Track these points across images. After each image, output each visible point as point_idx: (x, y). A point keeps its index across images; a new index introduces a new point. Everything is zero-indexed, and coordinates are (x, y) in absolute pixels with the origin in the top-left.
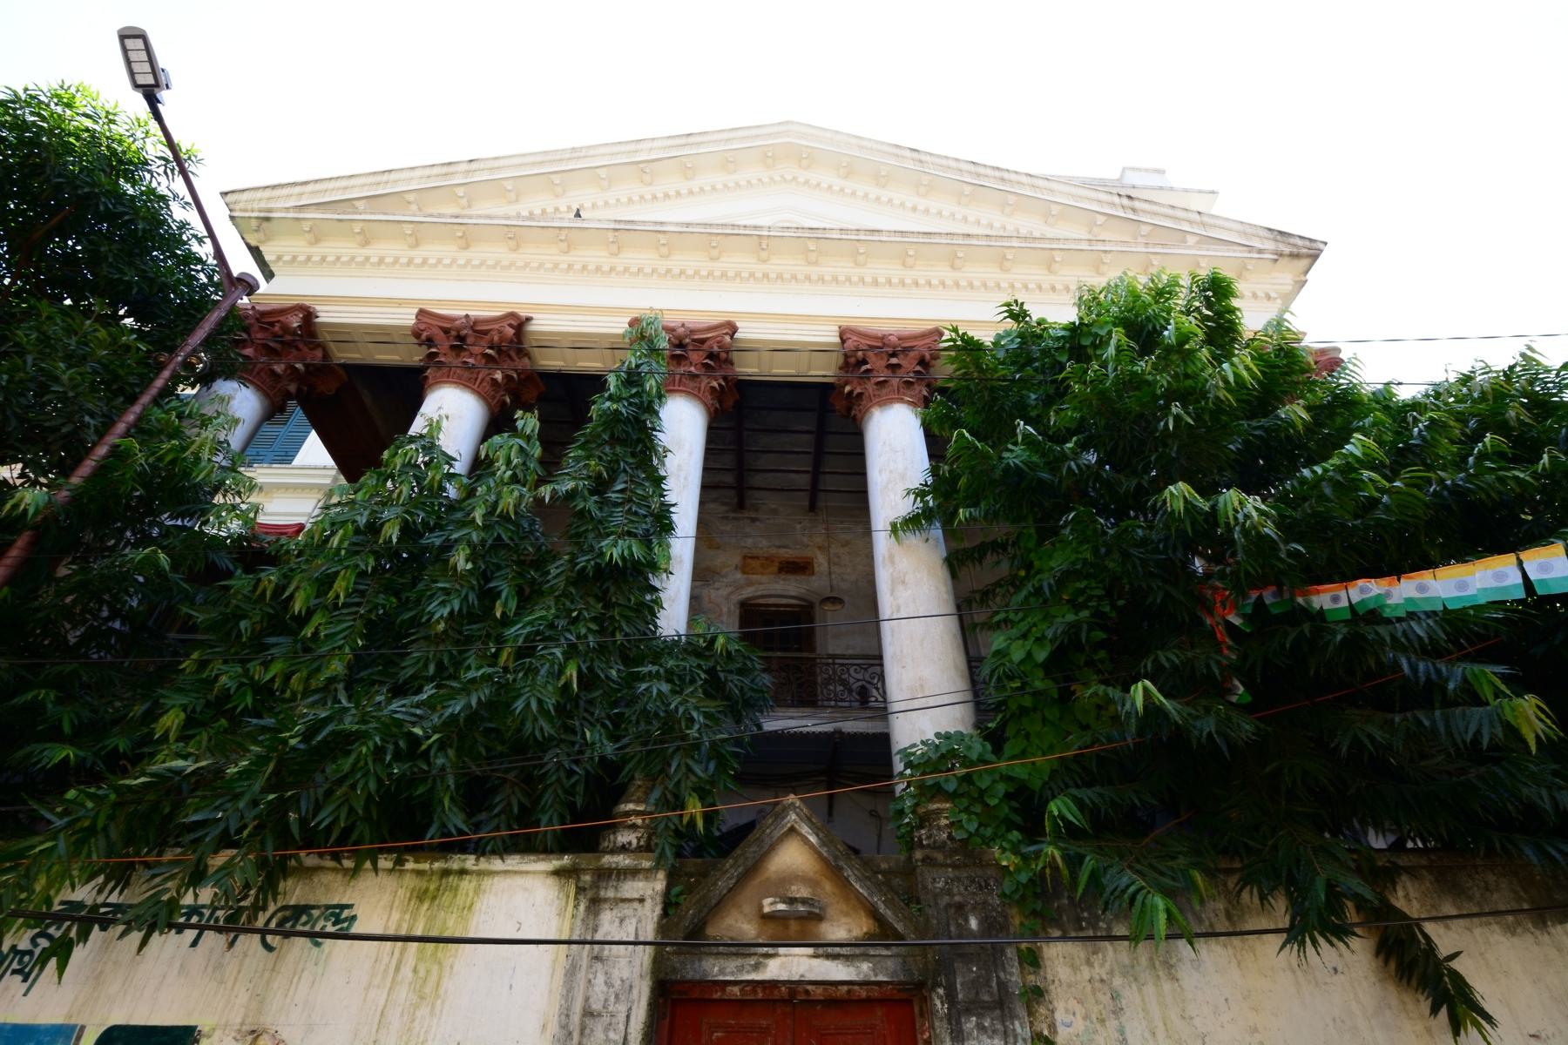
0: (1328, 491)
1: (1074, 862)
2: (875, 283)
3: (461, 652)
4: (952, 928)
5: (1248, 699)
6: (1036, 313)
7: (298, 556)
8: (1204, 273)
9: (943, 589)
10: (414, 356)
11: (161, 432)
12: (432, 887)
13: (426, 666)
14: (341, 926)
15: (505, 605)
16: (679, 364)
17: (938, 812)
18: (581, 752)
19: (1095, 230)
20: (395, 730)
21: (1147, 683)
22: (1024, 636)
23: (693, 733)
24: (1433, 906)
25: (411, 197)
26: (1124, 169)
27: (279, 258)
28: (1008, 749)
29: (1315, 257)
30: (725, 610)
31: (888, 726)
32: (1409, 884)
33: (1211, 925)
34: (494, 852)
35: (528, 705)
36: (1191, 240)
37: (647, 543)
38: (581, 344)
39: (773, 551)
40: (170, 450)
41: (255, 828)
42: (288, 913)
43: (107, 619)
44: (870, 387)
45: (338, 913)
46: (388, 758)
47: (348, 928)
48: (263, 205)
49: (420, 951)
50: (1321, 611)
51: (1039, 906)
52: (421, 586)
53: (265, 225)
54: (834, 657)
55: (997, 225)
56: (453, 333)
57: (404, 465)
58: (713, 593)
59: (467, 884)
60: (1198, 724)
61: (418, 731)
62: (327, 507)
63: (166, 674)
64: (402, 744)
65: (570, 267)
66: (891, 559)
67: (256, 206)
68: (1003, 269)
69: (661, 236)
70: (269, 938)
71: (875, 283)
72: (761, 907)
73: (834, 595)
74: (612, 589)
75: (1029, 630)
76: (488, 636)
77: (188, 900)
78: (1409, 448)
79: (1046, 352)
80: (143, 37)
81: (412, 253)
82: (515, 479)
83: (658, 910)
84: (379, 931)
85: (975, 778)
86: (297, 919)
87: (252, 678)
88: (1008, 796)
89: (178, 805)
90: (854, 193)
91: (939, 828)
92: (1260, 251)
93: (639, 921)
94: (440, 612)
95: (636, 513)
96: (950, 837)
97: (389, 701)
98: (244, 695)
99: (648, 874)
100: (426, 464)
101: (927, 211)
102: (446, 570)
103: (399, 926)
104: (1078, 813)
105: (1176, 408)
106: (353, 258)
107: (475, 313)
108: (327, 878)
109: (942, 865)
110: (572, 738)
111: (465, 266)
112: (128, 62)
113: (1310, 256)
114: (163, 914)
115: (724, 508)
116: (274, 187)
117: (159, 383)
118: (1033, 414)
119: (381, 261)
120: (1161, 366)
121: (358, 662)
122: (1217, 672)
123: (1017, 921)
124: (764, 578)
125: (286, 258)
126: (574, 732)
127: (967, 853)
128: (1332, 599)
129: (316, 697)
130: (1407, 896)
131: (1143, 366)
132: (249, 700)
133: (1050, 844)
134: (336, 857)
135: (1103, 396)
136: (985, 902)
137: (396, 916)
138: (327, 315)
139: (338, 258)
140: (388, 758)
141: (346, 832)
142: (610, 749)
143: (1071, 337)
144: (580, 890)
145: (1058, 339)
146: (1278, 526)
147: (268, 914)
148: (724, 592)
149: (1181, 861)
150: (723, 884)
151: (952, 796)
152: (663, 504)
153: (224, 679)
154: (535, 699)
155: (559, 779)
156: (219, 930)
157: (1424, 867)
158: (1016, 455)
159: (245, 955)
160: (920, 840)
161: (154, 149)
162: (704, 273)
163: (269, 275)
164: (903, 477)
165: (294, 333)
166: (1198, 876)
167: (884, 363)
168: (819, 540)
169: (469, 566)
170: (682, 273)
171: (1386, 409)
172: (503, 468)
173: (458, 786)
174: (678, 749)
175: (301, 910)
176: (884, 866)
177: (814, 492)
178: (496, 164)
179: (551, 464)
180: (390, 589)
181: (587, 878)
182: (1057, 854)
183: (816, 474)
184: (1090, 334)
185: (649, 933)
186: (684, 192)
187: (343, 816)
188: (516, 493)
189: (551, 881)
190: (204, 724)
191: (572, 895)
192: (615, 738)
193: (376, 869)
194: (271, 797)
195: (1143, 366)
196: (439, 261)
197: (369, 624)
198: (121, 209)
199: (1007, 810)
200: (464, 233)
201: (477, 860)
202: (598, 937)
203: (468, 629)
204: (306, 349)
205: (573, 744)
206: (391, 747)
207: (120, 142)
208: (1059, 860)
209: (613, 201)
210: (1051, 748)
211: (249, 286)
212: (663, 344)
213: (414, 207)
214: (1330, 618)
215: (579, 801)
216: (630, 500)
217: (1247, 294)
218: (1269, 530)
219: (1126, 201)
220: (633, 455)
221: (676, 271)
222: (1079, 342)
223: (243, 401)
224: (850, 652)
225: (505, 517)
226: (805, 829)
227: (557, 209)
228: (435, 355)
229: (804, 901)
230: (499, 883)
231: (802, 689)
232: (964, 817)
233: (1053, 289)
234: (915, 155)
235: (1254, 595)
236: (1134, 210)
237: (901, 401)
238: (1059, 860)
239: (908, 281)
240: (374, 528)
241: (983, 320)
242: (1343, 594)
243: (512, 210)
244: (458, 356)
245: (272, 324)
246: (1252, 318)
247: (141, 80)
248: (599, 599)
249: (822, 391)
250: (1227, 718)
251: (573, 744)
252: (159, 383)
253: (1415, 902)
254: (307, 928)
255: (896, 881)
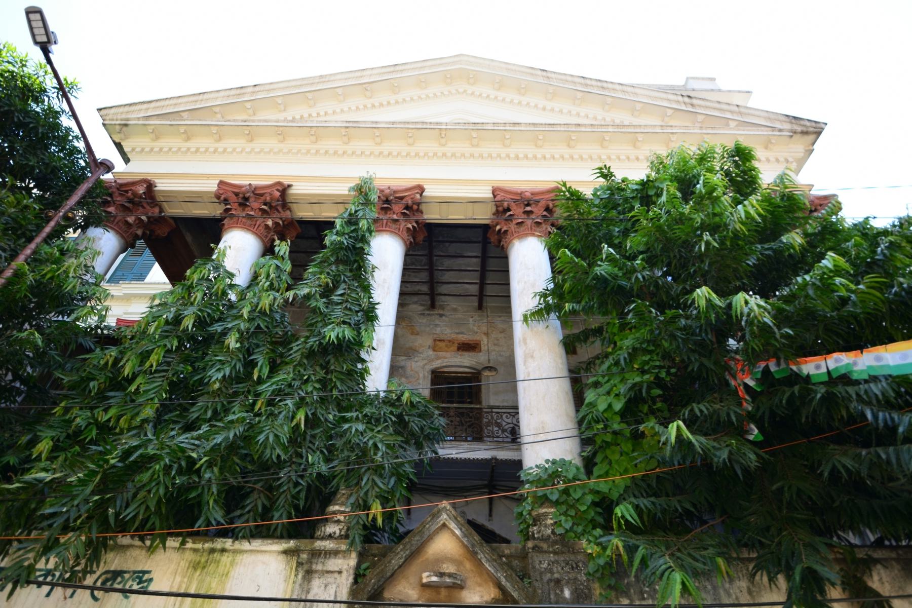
0: (811, 292)
1: (631, 550)
2: (517, 158)
3: (229, 403)
4: (552, 597)
5: (761, 438)
6: (619, 176)
7: (131, 339)
8: (731, 145)
9: (560, 361)
10: (216, 211)
11: (47, 260)
12: (203, 560)
13: (206, 411)
14: (142, 585)
15: (260, 371)
16: (386, 213)
17: (545, 515)
18: (305, 470)
19: (666, 119)
20: (180, 454)
21: (681, 423)
22: (608, 393)
23: (378, 458)
24: (900, 588)
25: (217, 109)
26: (687, 78)
27: (133, 150)
28: (596, 471)
29: (819, 133)
30: (421, 375)
31: (521, 455)
32: (882, 571)
33: (737, 598)
34: (244, 537)
35: (267, 438)
36: (732, 124)
37: (357, 327)
38: (317, 201)
39: (454, 336)
40: (49, 272)
41: (87, 518)
42: (109, 576)
43: (11, 381)
44: (512, 226)
45: (141, 576)
46: (173, 473)
47: (147, 587)
48: (124, 116)
49: (193, 603)
50: (808, 376)
51: (613, 582)
52: (207, 359)
53: (125, 129)
54: (492, 407)
55: (599, 117)
56: (241, 195)
57: (199, 280)
58: (414, 364)
59: (226, 559)
60: (718, 453)
61: (194, 455)
62: (151, 307)
63: (42, 417)
64: (183, 463)
65: (317, 152)
66: (525, 340)
67: (119, 117)
68: (603, 147)
69: (375, 130)
70: (96, 592)
71: (517, 158)
72: (421, 578)
73: (490, 365)
74: (332, 361)
75: (611, 389)
76: (249, 392)
77: (41, 565)
78: (875, 262)
79: (626, 200)
80: (39, 12)
81: (217, 145)
82: (271, 287)
83: (351, 579)
84: (166, 589)
85: (571, 491)
86: (114, 579)
87: (96, 420)
88: (594, 504)
89: (41, 502)
90: (504, 100)
91: (546, 526)
92: (780, 130)
93: (338, 586)
94: (216, 376)
95: (350, 309)
96: (553, 532)
97: (179, 435)
98: (91, 430)
99: (346, 554)
100: (215, 278)
101: (552, 110)
102: (222, 348)
103: (180, 586)
104: (636, 517)
105: (707, 236)
106: (180, 149)
107: (255, 183)
108: (135, 553)
109: (546, 552)
110: (300, 461)
111: (250, 152)
112: (31, 29)
113: (815, 133)
114: (24, 574)
115: (421, 308)
116: (131, 105)
117: (48, 229)
118: (616, 242)
119: (197, 150)
120: (697, 208)
121: (164, 408)
122: (734, 419)
123: (598, 592)
124: (448, 355)
125: (165, 150)
126: (302, 457)
127: (564, 543)
128: (814, 367)
129: (134, 432)
130: (880, 580)
131: (687, 209)
132: (94, 432)
133: (616, 537)
134: (142, 539)
135: (659, 228)
136: (576, 579)
137: (178, 579)
138: (162, 186)
139: (170, 149)
140: (173, 473)
141: (145, 521)
142: (324, 468)
143: (642, 190)
144: (299, 564)
145: (633, 191)
146: (774, 317)
147: (95, 576)
148: (421, 364)
149: (711, 551)
150: (395, 562)
151: (556, 503)
152: (370, 303)
153: (78, 420)
154: (274, 434)
155: (289, 488)
156: (64, 586)
157: (894, 559)
158: (602, 269)
159: (80, 603)
160: (533, 534)
161: (50, 83)
162: (404, 154)
163: (127, 160)
164: (533, 286)
165: (141, 197)
166: (720, 561)
167: (522, 210)
168: (484, 329)
169: (238, 345)
170: (390, 154)
171: (864, 235)
172: (264, 280)
173: (219, 492)
174: (369, 469)
175: (117, 574)
176: (507, 552)
177: (481, 296)
178: (272, 87)
179: (297, 277)
180: (186, 360)
181: (304, 556)
182: (620, 545)
183: (482, 285)
184: (655, 187)
185: (344, 595)
186: (392, 102)
187: (142, 512)
188: (271, 297)
189: (282, 558)
190: (64, 450)
191: (294, 568)
192: (328, 460)
193: (164, 548)
194: (96, 498)
195: (687, 209)
196: (234, 150)
197: (171, 384)
198: (28, 120)
199: (593, 514)
200: (250, 132)
201: (233, 542)
202: (310, 597)
203: (235, 387)
204: (148, 207)
205: (300, 464)
206: (176, 466)
207: (29, 78)
208: (621, 549)
209: (346, 109)
210: (626, 471)
211: (107, 166)
212: (374, 197)
213: (219, 116)
214: (814, 380)
215: (302, 503)
216: (347, 301)
217: (763, 159)
218: (768, 319)
219: (687, 100)
220: (351, 271)
221: (386, 153)
222: (646, 192)
223: (105, 241)
224: (505, 404)
225: (263, 313)
226: (452, 525)
227: (310, 115)
228: (230, 209)
229: (450, 575)
230: (247, 559)
231: (473, 426)
232: (563, 518)
233: (638, 159)
234: (544, 74)
235: (763, 365)
236: (692, 105)
237: (533, 235)
238: (621, 549)
239: (539, 156)
240: (178, 320)
241: (586, 183)
242: (823, 363)
243: (281, 116)
244: (244, 210)
245: (127, 192)
246: (767, 175)
247: (39, 39)
248: (322, 367)
249: (485, 228)
250: (745, 449)
251: (300, 464)
252: (48, 229)
253: (887, 584)
254: (120, 586)
255: (516, 563)
